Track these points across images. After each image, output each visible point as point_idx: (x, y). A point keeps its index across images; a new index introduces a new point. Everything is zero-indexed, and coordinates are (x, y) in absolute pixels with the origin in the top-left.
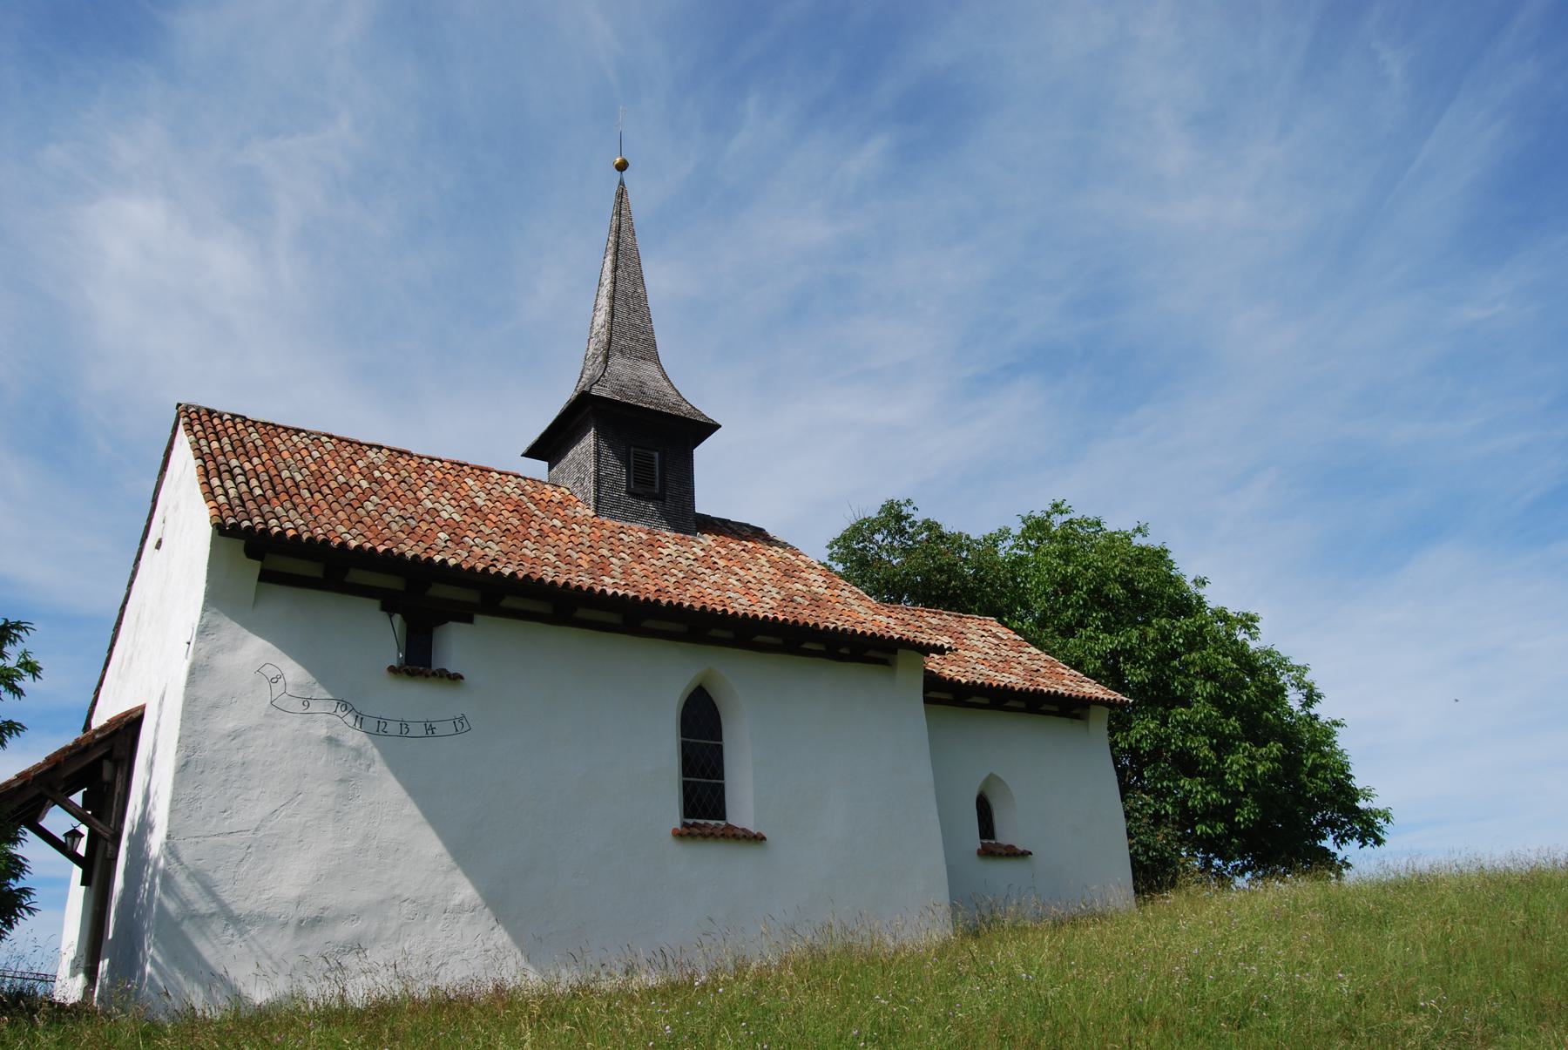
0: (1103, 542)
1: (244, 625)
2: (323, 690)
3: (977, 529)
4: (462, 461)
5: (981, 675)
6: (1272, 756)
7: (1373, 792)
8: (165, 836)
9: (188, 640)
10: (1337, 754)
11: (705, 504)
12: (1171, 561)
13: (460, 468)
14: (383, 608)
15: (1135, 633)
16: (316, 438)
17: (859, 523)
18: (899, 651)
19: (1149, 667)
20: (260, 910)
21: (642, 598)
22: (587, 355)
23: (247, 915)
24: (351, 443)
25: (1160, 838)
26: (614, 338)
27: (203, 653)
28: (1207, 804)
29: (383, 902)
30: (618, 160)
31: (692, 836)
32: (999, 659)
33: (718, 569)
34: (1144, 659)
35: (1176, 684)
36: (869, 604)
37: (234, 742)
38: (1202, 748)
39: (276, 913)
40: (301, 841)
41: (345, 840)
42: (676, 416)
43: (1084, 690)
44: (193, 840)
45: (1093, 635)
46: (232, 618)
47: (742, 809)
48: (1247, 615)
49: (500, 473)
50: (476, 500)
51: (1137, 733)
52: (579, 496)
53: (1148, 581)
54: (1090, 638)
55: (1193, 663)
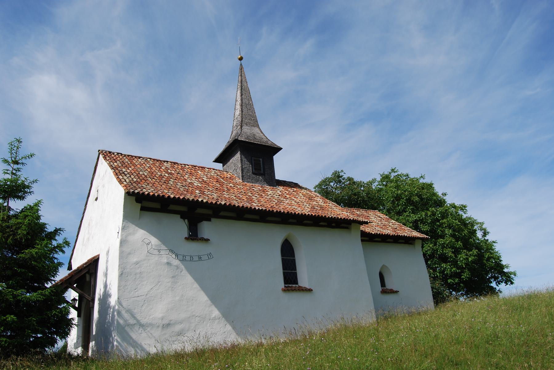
0: (410, 182)
1: (137, 225)
2: (164, 247)
3: (365, 180)
4: (195, 165)
5: (378, 231)
6: (474, 254)
7: (509, 265)
8: (117, 298)
9: (118, 232)
10: (496, 253)
11: (279, 176)
12: (433, 187)
13: (195, 168)
14: (181, 218)
15: (424, 213)
16: (146, 159)
17: (325, 179)
18: (352, 224)
19: (429, 225)
20: (150, 322)
21: (268, 210)
22: (233, 126)
23: (146, 324)
24: (158, 161)
25: (437, 285)
26: (243, 120)
27: (124, 236)
28: (452, 272)
29: (189, 317)
30: (239, 57)
31: (288, 290)
32: (383, 225)
33: (287, 198)
34: (427, 222)
35: (439, 231)
36: (339, 208)
37: (137, 265)
38: (449, 253)
39: (155, 323)
40: (161, 298)
41: (176, 297)
42: (267, 146)
43: (413, 234)
44: (127, 299)
45: (408, 215)
46: (133, 224)
47: (303, 280)
48: (463, 205)
49: (208, 169)
50: (203, 178)
51: (426, 249)
52: (236, 175)
53: (427, 195)
54: (408, 216)
55: (444, 223)
